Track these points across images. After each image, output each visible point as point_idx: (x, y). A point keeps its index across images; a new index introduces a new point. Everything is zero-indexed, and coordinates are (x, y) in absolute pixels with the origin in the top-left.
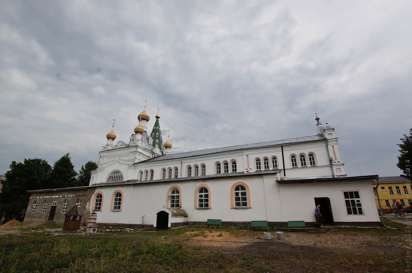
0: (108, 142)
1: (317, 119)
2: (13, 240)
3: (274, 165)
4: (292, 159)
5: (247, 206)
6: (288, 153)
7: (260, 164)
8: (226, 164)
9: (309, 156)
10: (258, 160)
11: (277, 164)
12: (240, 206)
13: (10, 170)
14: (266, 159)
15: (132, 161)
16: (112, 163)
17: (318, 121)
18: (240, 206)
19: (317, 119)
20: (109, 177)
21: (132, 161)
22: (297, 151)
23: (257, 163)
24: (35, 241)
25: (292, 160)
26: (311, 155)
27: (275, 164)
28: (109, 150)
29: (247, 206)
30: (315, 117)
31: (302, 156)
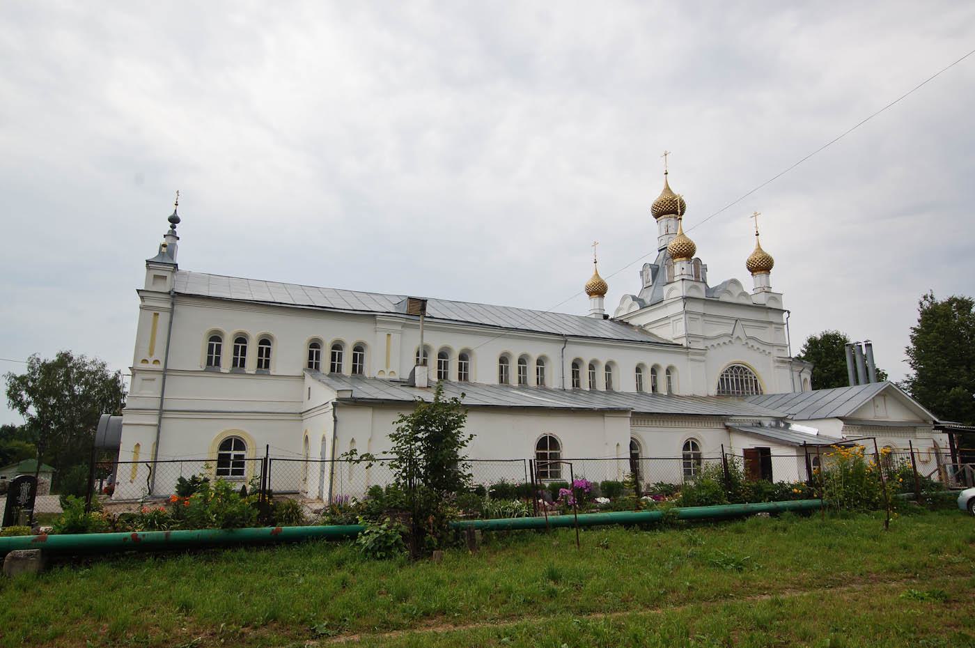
0: (768, 282)
1: (174, 220)
2: (846, 543)
3: (441, 372)
4: (260, 348)
5: (243, 475)
6: (574, 351)
7: (244, 353)
8: (241, 340)
9: (260, 344)
10: (216, 338)
11: (233, 356)
12: (547, 478)
13: (819, 338)
14: (337, 346)
15: (780, 348)
16: (726, 340)
17: (173, 227)
18: (228, 475)
19: (174, 220)
20: (722, 380)
21: (780, 348)
22: (329, 332)
23: (211, 347)
24: (45, 583)
25: (311, 353)
26: (265, 341)
27: (264, 358)
28: (771, 308)
29: (243, 475)
30: (171, 213)
31: (241, 340)
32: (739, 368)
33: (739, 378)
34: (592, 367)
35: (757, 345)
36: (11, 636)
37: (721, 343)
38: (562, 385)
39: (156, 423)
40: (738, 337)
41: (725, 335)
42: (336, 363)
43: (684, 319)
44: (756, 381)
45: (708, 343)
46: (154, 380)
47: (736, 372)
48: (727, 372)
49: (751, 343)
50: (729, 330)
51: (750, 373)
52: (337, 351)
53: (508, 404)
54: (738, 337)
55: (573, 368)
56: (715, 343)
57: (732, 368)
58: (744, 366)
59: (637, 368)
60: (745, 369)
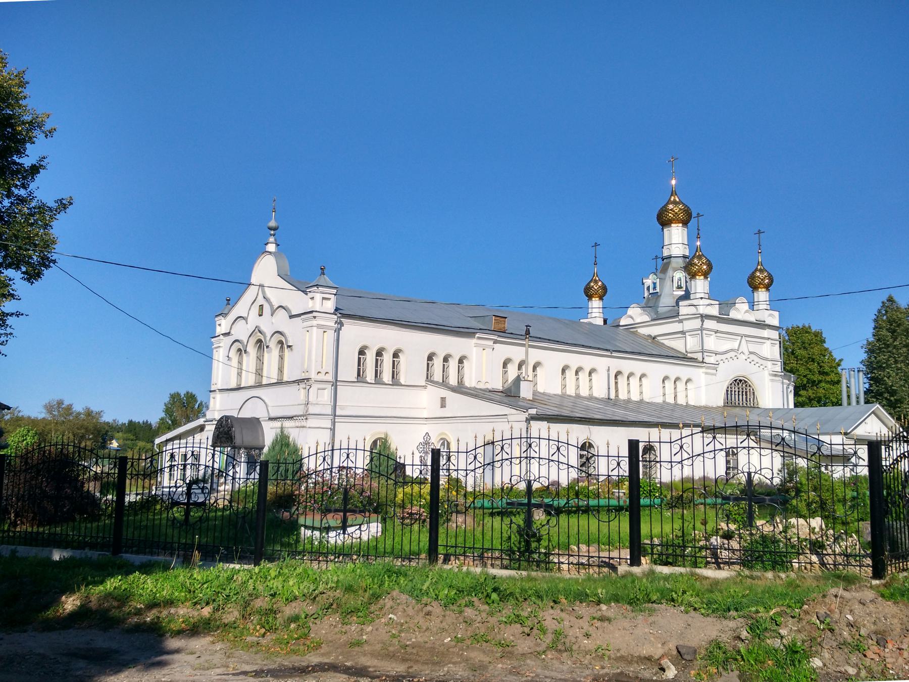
20: (727, 391)
32: (741, 381)
33: (744, 390)
34: (446, 359)
35: (756, 359)
36: (671, 673)
37: (729, 358)
38: (330, 369)
39: (329, 426)
40: (742, 352)
41: (732, 350)
42: (379, 369)
43: (738, 341)
44: (754, 393)
45: (719, 357)
46: (324, 389)
47: (738, 384)
48: (731, 384)
49: (752, 357)
50: (735, 345)
51: (750, 386)
52: (379, 358)
53: (608, 418)
54: (742, 352)
55: (359, 355)
56: (724, 357)
57: (736, 381)
58: (746, 380)
59: (504, 363)
60: (746, 382)
